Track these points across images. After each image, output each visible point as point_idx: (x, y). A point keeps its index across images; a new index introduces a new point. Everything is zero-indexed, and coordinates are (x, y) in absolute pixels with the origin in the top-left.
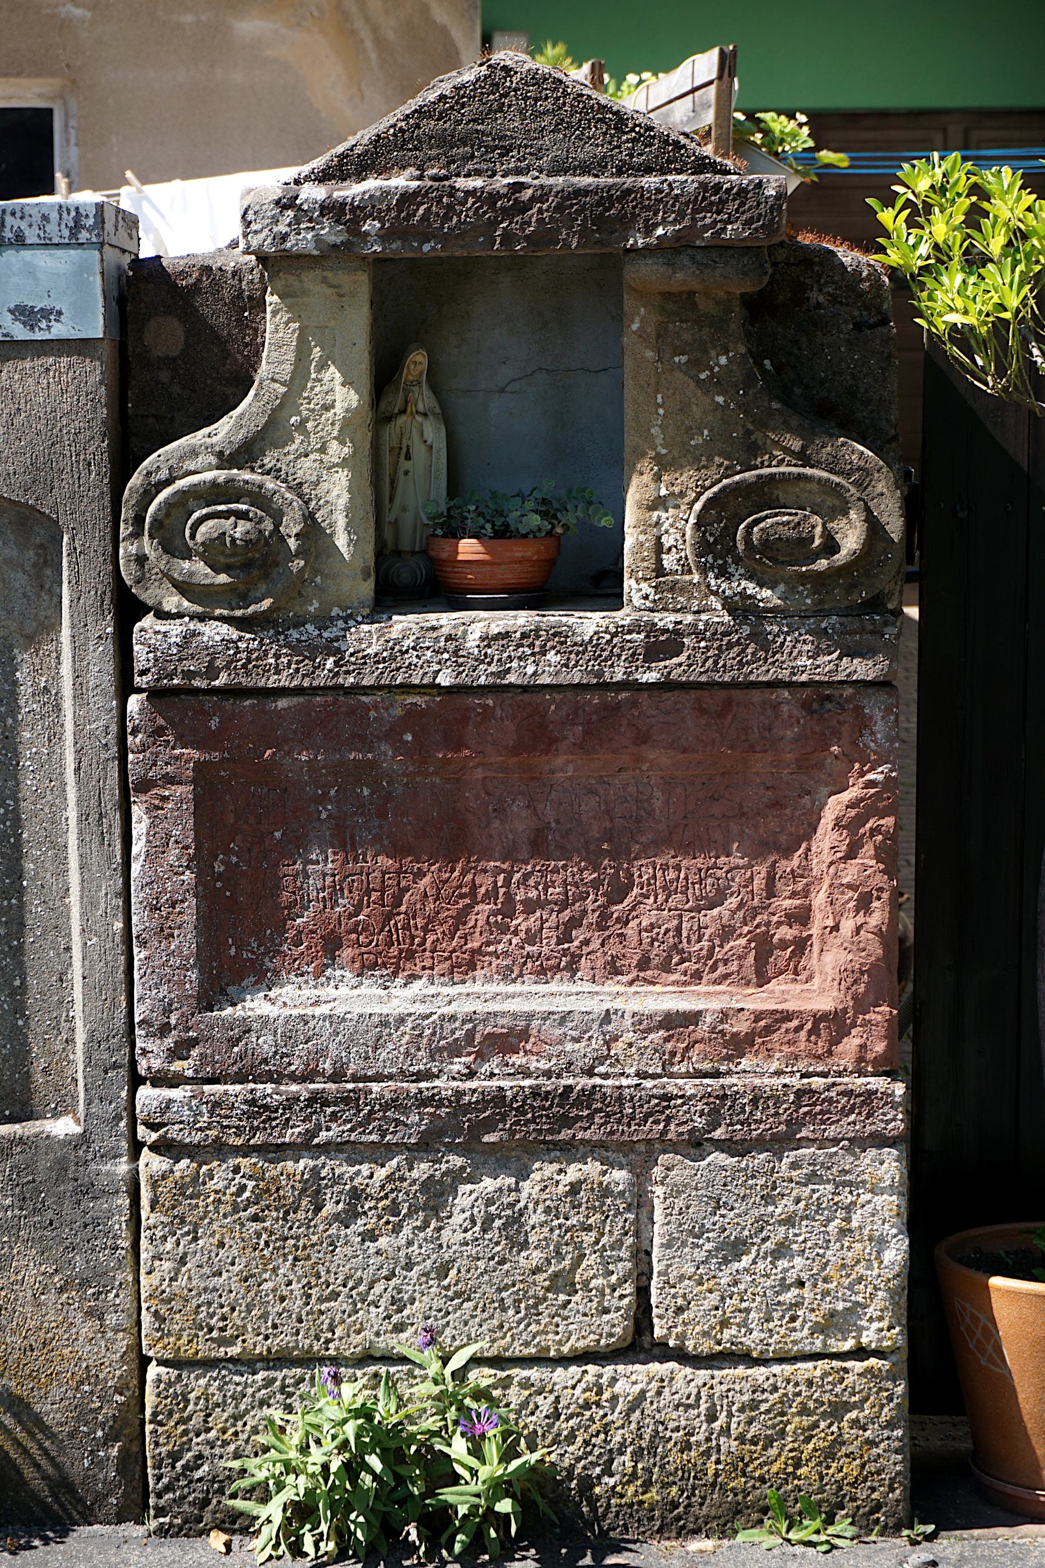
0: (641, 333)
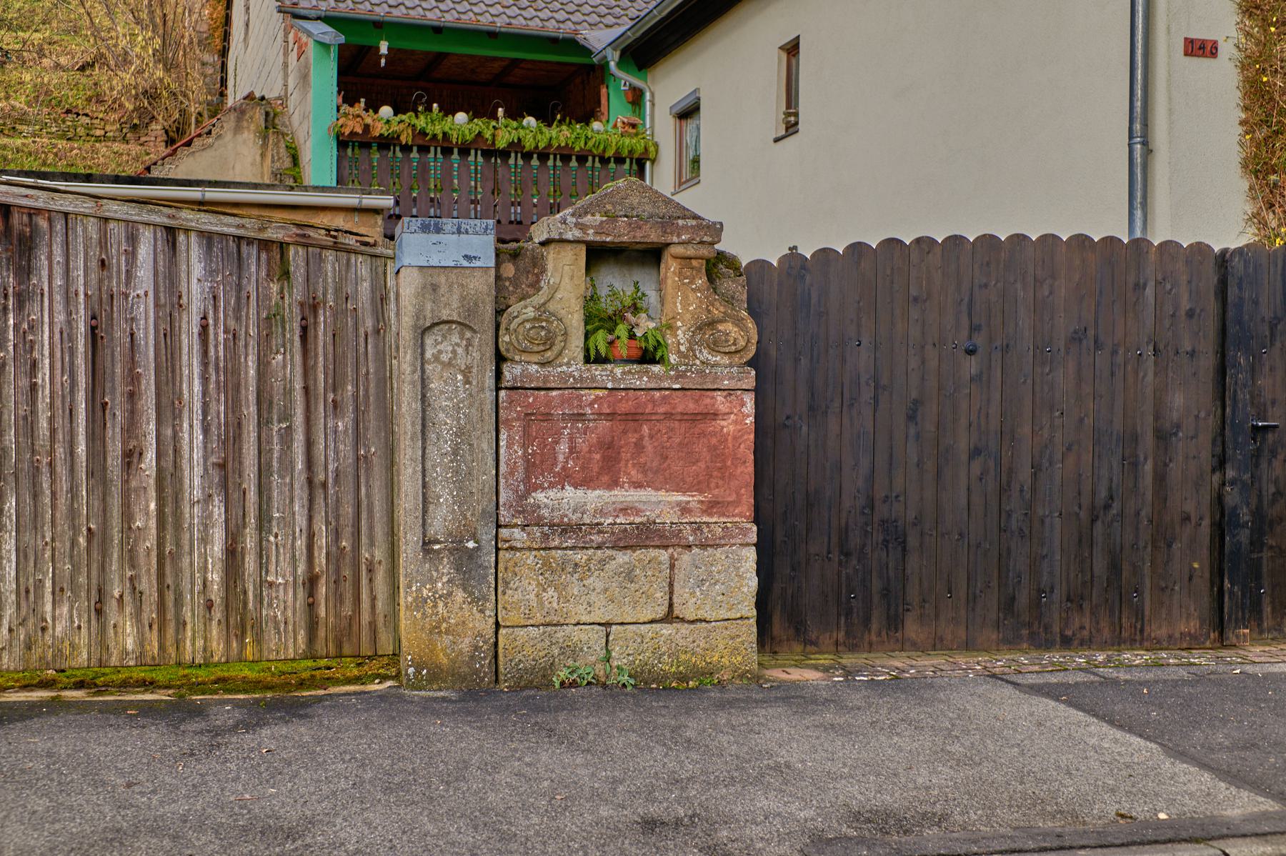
0: (674, 272)
